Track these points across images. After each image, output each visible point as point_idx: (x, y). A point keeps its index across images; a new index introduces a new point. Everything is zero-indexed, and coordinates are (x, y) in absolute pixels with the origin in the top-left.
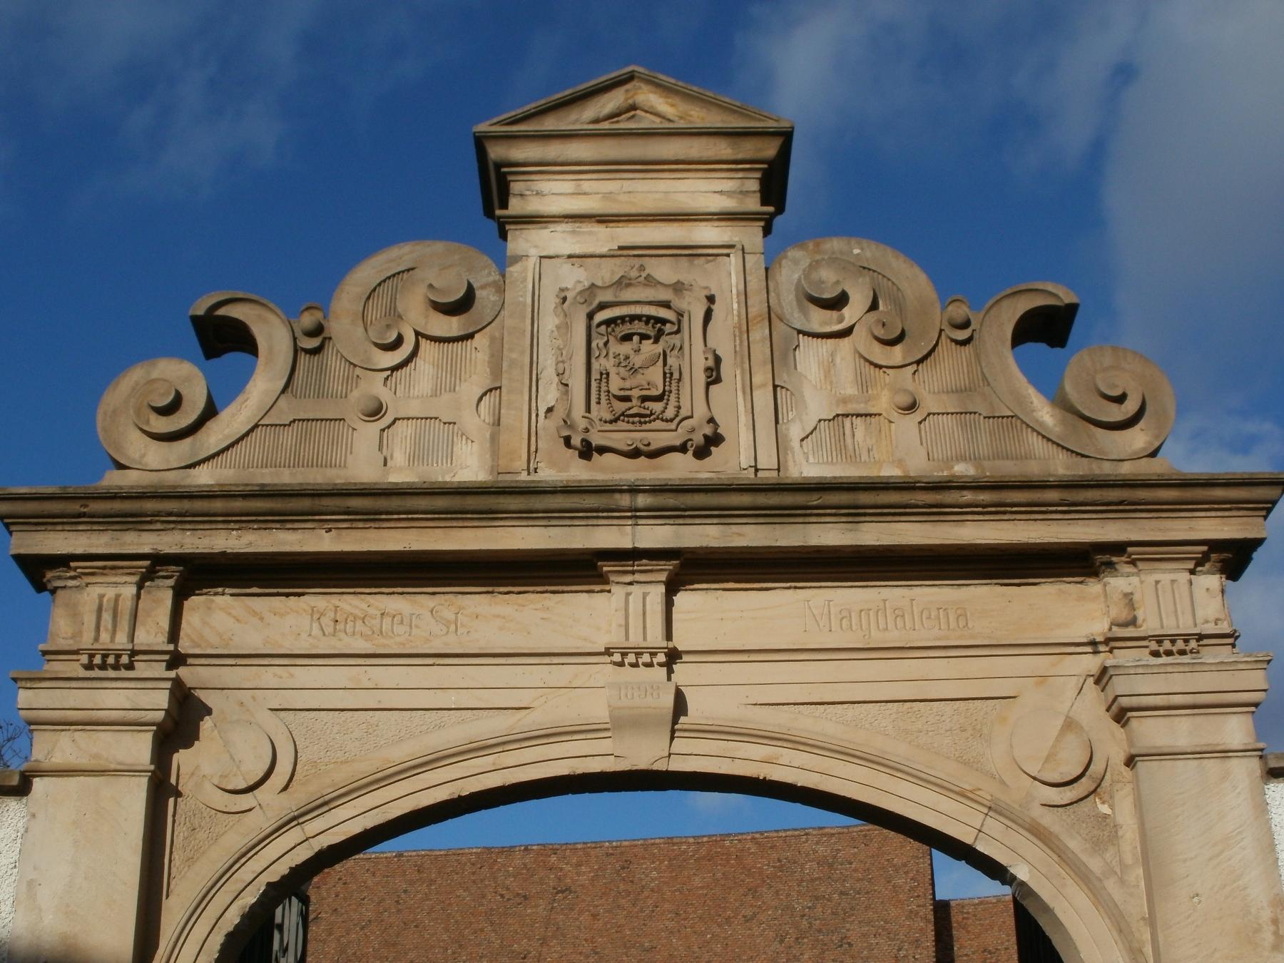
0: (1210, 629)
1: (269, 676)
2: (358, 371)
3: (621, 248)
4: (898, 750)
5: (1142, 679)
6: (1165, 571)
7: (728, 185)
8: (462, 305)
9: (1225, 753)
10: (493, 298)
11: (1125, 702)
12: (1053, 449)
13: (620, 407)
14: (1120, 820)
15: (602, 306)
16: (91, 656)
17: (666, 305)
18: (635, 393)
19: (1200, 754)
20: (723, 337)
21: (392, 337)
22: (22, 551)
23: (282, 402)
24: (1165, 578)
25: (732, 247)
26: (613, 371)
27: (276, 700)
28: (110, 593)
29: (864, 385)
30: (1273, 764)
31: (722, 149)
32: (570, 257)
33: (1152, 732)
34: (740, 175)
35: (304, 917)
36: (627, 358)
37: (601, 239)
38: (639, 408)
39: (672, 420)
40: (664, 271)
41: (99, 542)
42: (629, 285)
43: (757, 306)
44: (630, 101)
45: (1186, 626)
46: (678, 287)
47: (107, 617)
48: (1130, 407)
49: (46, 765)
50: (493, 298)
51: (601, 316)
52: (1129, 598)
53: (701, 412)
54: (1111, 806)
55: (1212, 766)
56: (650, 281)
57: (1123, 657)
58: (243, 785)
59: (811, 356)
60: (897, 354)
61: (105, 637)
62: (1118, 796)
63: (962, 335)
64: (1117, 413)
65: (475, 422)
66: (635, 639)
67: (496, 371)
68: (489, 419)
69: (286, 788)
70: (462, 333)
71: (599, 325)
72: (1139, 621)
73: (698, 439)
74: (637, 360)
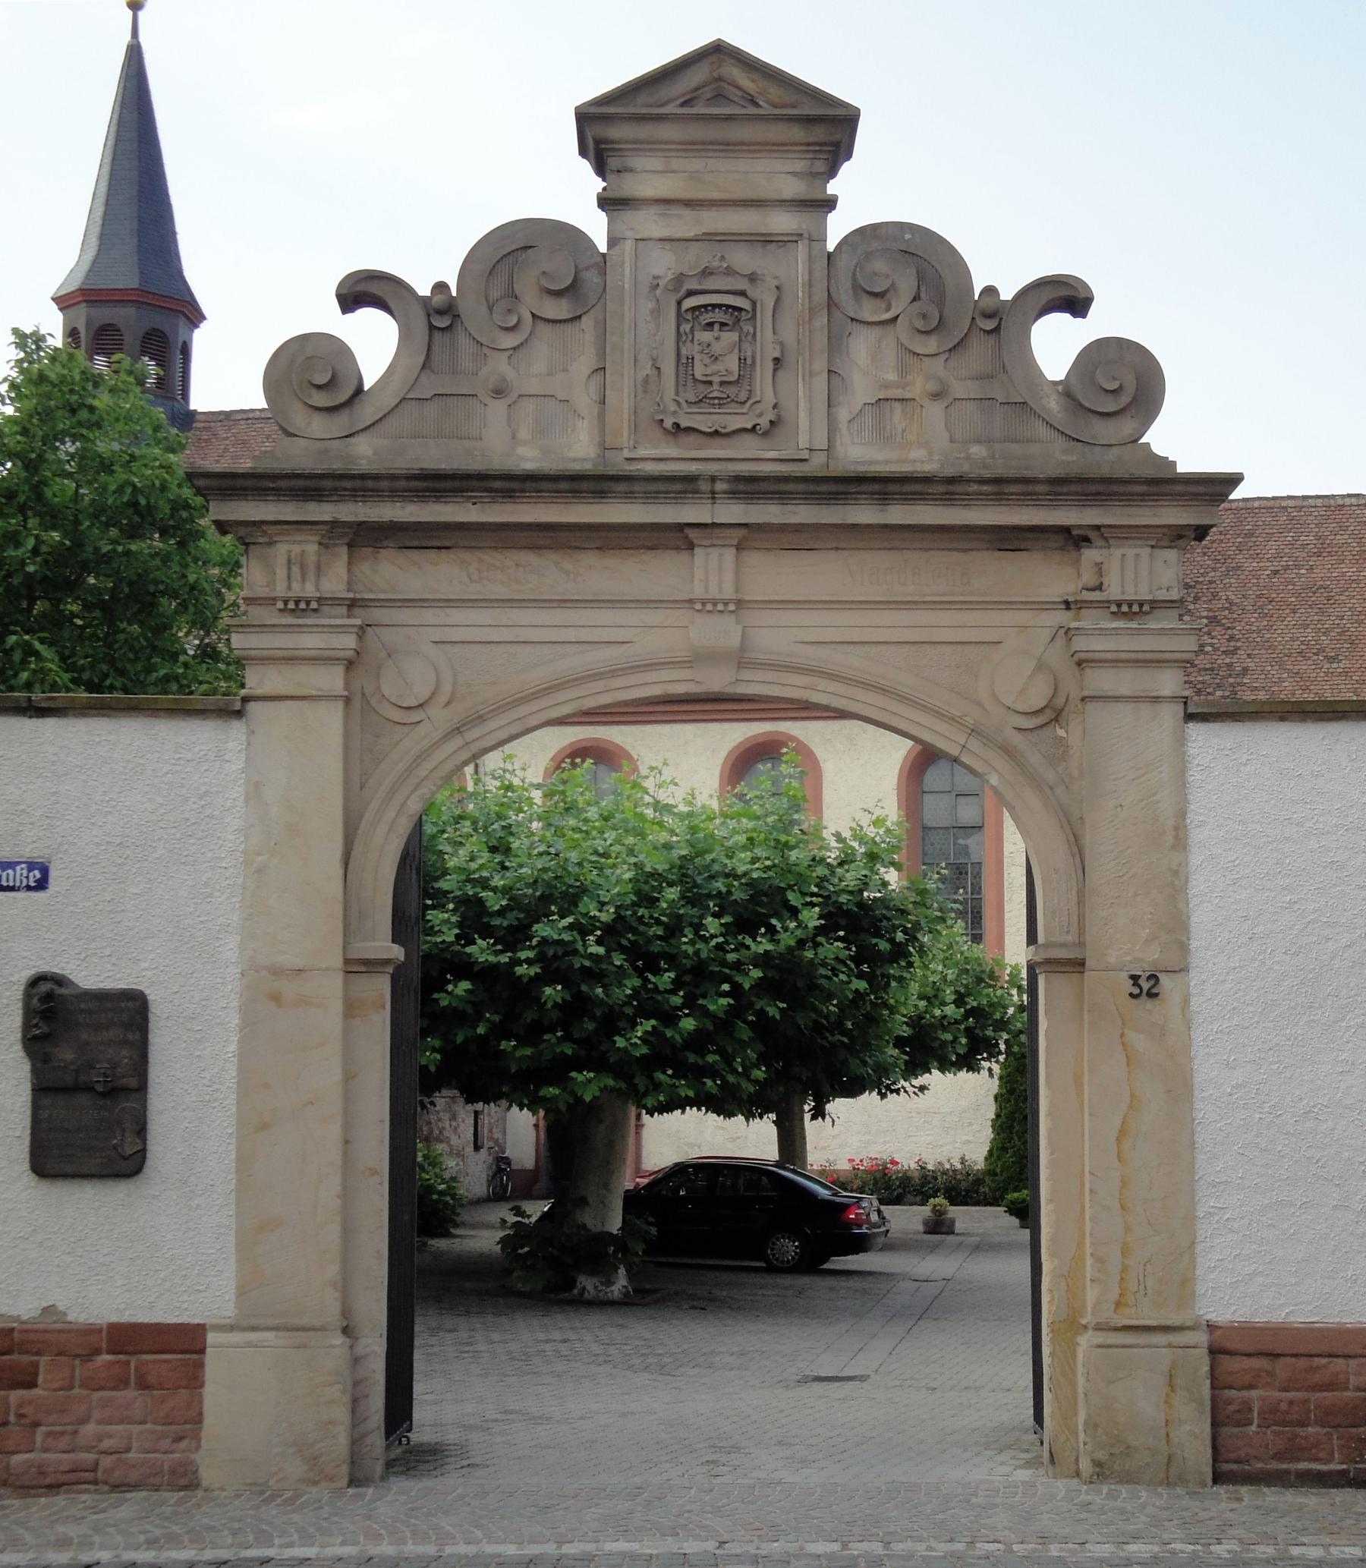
0: (1162, 595)
1: (429, 616)
2: (485, 350)
5: (1102, 635)
6: (1130, 547)
8: (573, 290)
9: (1156, 699)
11: (1083, 656)
12: (1054, 435)
13: (703, 390)
15: (691, 293)
16: (286, 602)
17: (742, 293)
18: (716, 379)
19: (1136, 699)
20: (789, 332)
21: (513, 321)
23: (424, 379)
25: (801, 235)
26: (697, 357)
27: (438, 635)
28: (296, 549)
29: (903, 372)
30: (1191, 710)
31: (797, 133)
32: (661, 240)
33: (1102, 680)
35: (476, 772)
37: (686, 224)
40: (742, 259)
42: (711, 274)
43: (821, 296)
44: (715, 74)
45: (1144, 595)
46: (752, 278)
47: (296, 569)
48: (1125, 399)
49: (259, 692)
51: (689, 303)
52: (1099, 566)
53: (769, 398)
55: (1145, 708)
56: (730, 272)
57: (1088, 620)
58: (415, 703)
59: (861, 345)
60: (931, 345)
61: (296, 586)
63: (989, 325)
65: (584, 401)
66: (713, 593)
67: (602, 354)
68: (596, 397)
69: (448, 703)
73: (764, 422)
74: (717, 348)
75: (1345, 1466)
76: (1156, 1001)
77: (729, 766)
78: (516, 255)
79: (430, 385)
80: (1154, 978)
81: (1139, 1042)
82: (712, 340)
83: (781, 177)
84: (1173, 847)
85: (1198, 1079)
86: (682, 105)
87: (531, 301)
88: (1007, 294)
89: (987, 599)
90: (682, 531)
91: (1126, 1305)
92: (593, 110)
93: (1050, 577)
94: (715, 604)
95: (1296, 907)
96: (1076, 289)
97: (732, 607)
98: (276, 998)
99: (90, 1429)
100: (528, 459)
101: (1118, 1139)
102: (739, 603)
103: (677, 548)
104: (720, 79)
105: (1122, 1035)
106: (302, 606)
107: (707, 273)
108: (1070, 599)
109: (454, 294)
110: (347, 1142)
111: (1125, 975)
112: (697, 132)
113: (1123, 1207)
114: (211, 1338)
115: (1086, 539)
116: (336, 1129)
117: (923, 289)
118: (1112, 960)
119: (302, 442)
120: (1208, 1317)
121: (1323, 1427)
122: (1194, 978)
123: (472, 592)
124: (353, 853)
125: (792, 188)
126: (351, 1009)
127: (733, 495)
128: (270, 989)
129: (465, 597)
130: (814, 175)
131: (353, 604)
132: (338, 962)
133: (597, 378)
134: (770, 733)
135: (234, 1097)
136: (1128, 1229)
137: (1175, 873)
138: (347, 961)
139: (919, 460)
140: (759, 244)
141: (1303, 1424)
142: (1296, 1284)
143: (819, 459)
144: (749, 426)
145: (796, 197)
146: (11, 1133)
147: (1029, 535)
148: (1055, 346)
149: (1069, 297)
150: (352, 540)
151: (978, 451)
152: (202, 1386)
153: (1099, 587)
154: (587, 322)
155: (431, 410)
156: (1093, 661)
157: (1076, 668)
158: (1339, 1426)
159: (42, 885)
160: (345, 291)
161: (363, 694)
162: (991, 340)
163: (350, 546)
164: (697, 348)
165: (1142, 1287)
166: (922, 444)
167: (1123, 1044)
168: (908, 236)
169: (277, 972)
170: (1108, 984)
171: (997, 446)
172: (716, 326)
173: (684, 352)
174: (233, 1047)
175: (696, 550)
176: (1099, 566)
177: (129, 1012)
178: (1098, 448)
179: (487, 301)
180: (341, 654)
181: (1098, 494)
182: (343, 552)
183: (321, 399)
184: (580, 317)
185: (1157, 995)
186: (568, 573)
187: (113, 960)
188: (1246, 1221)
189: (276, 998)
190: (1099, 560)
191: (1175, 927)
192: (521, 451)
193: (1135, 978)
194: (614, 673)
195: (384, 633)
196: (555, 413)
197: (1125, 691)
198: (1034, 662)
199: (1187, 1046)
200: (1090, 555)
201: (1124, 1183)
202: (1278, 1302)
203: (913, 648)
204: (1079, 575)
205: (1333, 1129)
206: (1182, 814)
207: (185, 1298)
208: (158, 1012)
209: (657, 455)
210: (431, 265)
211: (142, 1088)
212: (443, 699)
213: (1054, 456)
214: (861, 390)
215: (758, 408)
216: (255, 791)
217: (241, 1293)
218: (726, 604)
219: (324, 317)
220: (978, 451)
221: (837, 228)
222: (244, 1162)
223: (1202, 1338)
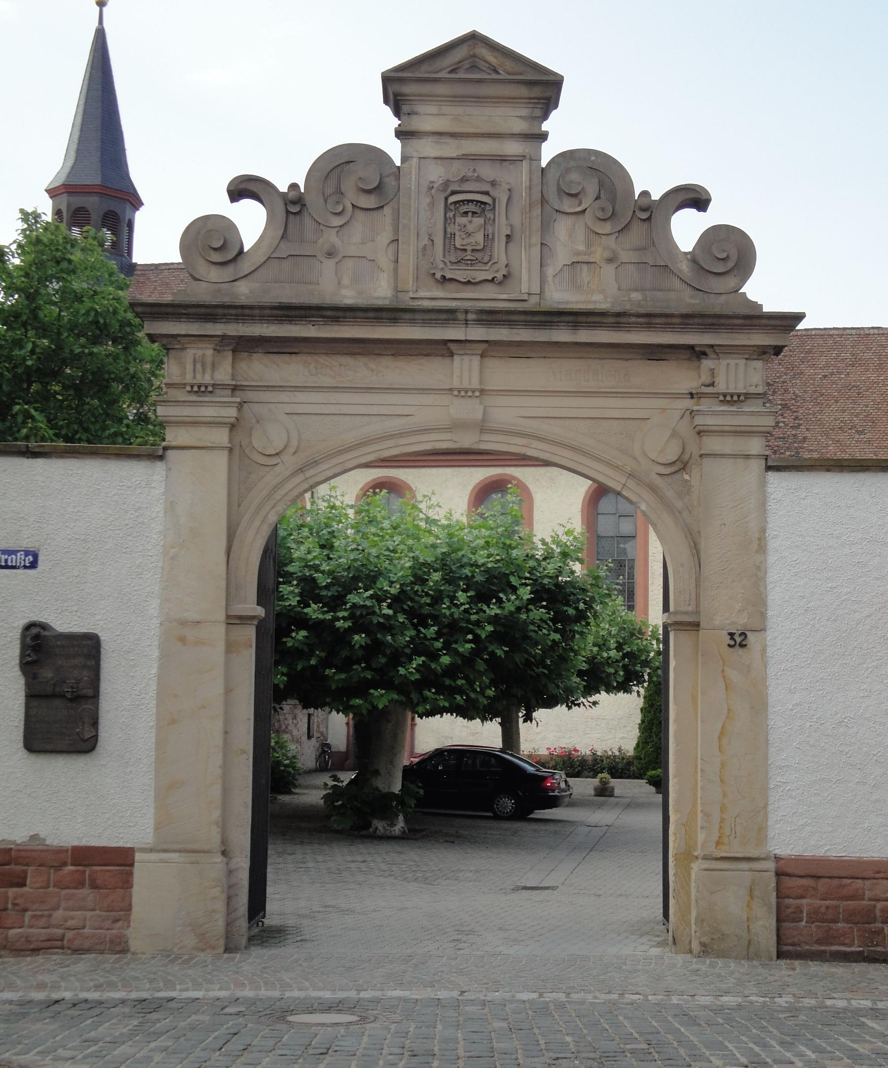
0: (752, 390)
1: (284, 397)
2: (322, 227)
5: (714, 415)
6: (732, 358)
7: (524, 112)
8: (378, 190)
9: (748, 457)
10: (393, 183)
11: (701, 428)
12: (684, 286)
13: (460, 255)
15: (454, 193)
16: (192, 387)
17: (487, 193)
18: (469, 248)
22: (151, 332)
23: (282, 245)
24: (732, 362)
26: (457, 233)
27: (289, 409)
28: (199, 353)
29: (589, 244)
30: (770, 464)
31: (523, 91)
33: (713, 444)
34: (532, 106)
35: (312, 497)
37: (451, 149)
39: (487, 263)
40: (487, 171)
41: (194, 328)
42: (467, 180)
43: (537, 196)
44: (471, 53)
46: (493, 183)
47: (199, 366)
48: (730, 264)
50: (393, 183)
51: (453, 199)
52: (712, 371)
53: (503, 260)
55: (741, 462)
56: (479, 179)
58: (274, 452)
59: (562, 228)
60: (607, 228)
61: (198, 376)
64: (721, 268)
65: (385, 260)
66: (466, 385)
67: (396, 230)
68: (393, 258)
69: (295, 453)
73: (499, 276)
74: (470, 228)
76: (745, 650)
78: (343, 167)
79: (286, 249)
81: (733, 675)
83: (512, 119)
85: (771, 700)
88: (656, 196)
91: (723, 844)
92: (393, 74)
93: (682, 377)
94: (466, 392)
95: (835, 591)
97: (477, 394)
98: (182, 640)
99: (59, 914)
100: (348, 297)
101: (719, 738)
102: (482, 391)
103: (443, 356)
104: (474, 56)
105: (723, 671)
106: (203, 389)
107: (464, 180)
110: (226, 732)
112: (459, 90)
113: (722, 781)
114: (138, 856)
115: (705, 354)
116: (219, 725)
117: (602, 192)
120: (775, 852)
121: (848, 923)
122: (770, 635)
125: (520, 126)
126: (230, 647)
127: (479, 322)
128: (179, 634)
130: (534, 118)
132: (222, 617)
136: (725, 795)
137: (758, 568)
138: (228, 617)
139: (598, 301)
141: (835, 921)
143: (534, 300)
146: (11, 724)
147: (668, 350)
148: (686, 229)
149: (695, 198)
151: (636, 296)
153: (712, 384)
154: (387, 210)
158: (858, 923)
159: (33, 565)
160: (232, 188)
162: (645, 225)
164: (457, 227)
166: (600, 291)
168: (593, 158)
169: (183, 623)
171: (648, 293)
172: (470, 214)
173: (449, 230)
174: (154, 671)
175: (455, 357)
176: (712, 371)
177: (89, 647)
180: (227, 420)
182: (229, 355)
183: (216, 257)
186: (372, 370)
187: (79, 614)
189: (182, 640)
191: (758, 603)
192: (344, 292)
193: (731, 635)
196: (366, 268)
198: (670, 432)
199: (765, 679)
200: (707, 364)
201: (723, 766)
202: (820, 843)
206: (763, 530)
208: (107, 648)
209: (431, 295)
210: (288, 172)
211: (96, 696)
212: (291, 450)
213: (685, 300)
214: (562, 256)
215: (496, 267)
216: (170, 508)
217: (157, 828)
218: (473, 392)
219: (220, 205)
220: (636, 296)
221: (548, 152)
222: (160, 745)
223: (771, 865)
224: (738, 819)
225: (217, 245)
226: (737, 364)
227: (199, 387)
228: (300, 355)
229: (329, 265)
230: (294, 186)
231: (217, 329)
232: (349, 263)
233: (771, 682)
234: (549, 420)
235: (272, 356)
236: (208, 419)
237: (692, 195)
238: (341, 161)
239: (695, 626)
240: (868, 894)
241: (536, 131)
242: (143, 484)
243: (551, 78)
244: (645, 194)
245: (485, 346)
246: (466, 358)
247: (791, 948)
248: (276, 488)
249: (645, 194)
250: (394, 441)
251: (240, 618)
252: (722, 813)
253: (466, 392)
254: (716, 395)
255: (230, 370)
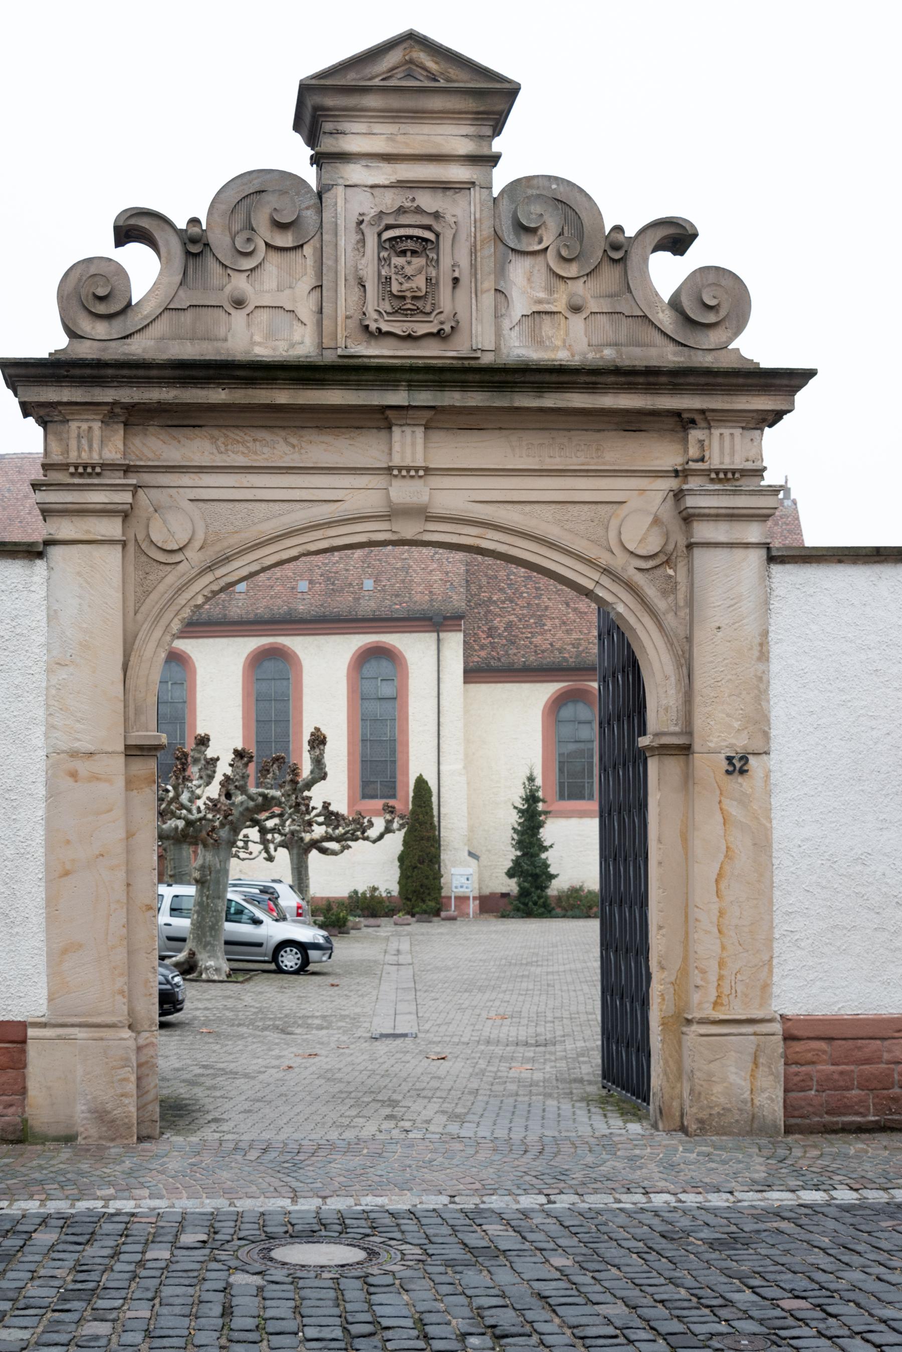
1: (186, 479)
2: (229, 271)
3: (399, 181)
4: (553, 532)
6: (726, 427)
9: (747, 545)
12: (666, 341)
13: (397, 304)
14: (679, 579)
15: (388, 227)
16: (76, 468)
17: (428, 228)
24: (726, 432)
25: (473, 183)
26: (394, 277)
28: (85, 426)
31: (469, 104)
36: (403, 268)
37: (383, 174)
38: (406, 304)
39: (429, 314)
40: (428, 201)
42: (405, 212)
46: (437, 215)
47: (84, 442)
52: (701, 442)
54: (675, 571)
56: (419, 210)
58: (176, 547)
60: (572, 270)
62: (679, 565)
66: (408, 462)
67: (320, 274)
69: (201, 548)
70: (296, 244)
71: (385, 241)
72: (706, 458)
74: (409, 270)
75: (877, 1118)
76: (746, 776)
77: (355, 657)
78: (250, 194)
79: (184, 299)
80: (744, 759)
81: (734, 810)
82: (405, 263)
83: (455, 138)
84: (759, 659)
85: (776, 835)
86: (383, 80)
87: (265, 232)
88: (630, 232)
89: (617, 468)
90: (383, 413)
91: (722, 1005)
92: (313, 82)
93: (664, 454)
94: (408, 471)
95: (849, 704)
96: (684, 228)
97: (421, 473)
98: (74, 775)
101: (716, 881)
102: (427, 470)
103: (379, 428)
104: (411, 61)
105: (720, 802)
106: (89, 470)
107: (401, 211)
108: (679, 468)
109: (204, 227)
110: (128, 885)
111: (723, 756)
112: (395, 102)
113: (720, 932)
114: (31, 1032)
115: (693, 422)
116: (121, 874)
117: (566, 228)
118: (711, 745)
119: (88, 343)
120: (781, 1012)
121: (863, 1090)
123: (219, 461)
124: (130, 664)
125: (465, 147)
126: (129, 783)
129: (214, 464)
130: (481, 137)
131: (127, 470)
132: (121, 748)
133: (316, 294)
134: (377, 642)
135: (43, 850)
136: (723, 948)
137: (760, 679)
138: (127, 747)
140: (440, 190)
141: (848, 1089)
142: (847, 986)
144: (435, 330)
145: (470, 153)
147: (648, 418)
148: (666, 274)
149: (676, 237)
150: (127, 420)
152: (25, 1066)
153: (702, 460)
155: (188, 317)
156: (699, 515)
157: (682, 522)
158: (875, 1089)
160: (121, 223)
161: (136, 540)
162: (618, 269)
163: (126, 424)
164: (393, 270)
165: (733, 991)
166: (570, 343)
167: (721, 809)
168: (554, 186)
169: (74, 754)
170: (708, 766)
171: (624, 349)
172: (409, 254)
173: (383, 273)
174: (41, 813)
175: (394, 429)
176: (701, 442)
178: (700, 352)
179: (230, 233)
180: (120, 507)
181: (707, 384)
182: (120, 429)
184: (302, 246)
185: (747, 771)
186: (294, 446)
188: (810, 941)
190: (701, 438)
191: (760, 723)
193: (730, 759)
194: (329, 524)
195: (153, 493)
196: (277, 316)
197: (722, 538)
198: (652, 517)
199: (768, 810)
200: (695, 434)
201: (721, 914)
202: (832, 1000)
203: (559, 506)
204: (686, 450)
205: (875, 871)
206: (765, 634)
207: (10, 1002)
210: (186, 202)
212: (197, 544)
214: (520, 306)
215: (442, 317)
216: (52, 617)
217: (50, 999)
218: (417, 471)
219: (103, 244)
220: (609, 353)
221: (501, 177)
222: (51, 902)
223: (777, 1027)
224: (739, 976)
225: (101, 292)
226: (721, 434)
227: (85, 468)
228: (206, 429)
229: (238, 317)
230: (194, 221)
231: (108, 395)
232: (263, 316)
233: (776, 814)
234: (506, 505)
235: (170, 430)
236: (99, 507)
237: (671, 231)
238: (251, 191)
239: (685, 750)
240: (886, 1056)
241: (485, 152)
242: (20, 587)
243: (507, 85)
244: (618, 229)
245: (429, 414)
246: (408, 430)
247: (799, 1121)
248: (180, 590)
249: (618, 229)
250: (321, 532)
251: (140, 747)
252: (720, 969)
253: (408, 471)
254: (706, 473)
255: (120, 446)
